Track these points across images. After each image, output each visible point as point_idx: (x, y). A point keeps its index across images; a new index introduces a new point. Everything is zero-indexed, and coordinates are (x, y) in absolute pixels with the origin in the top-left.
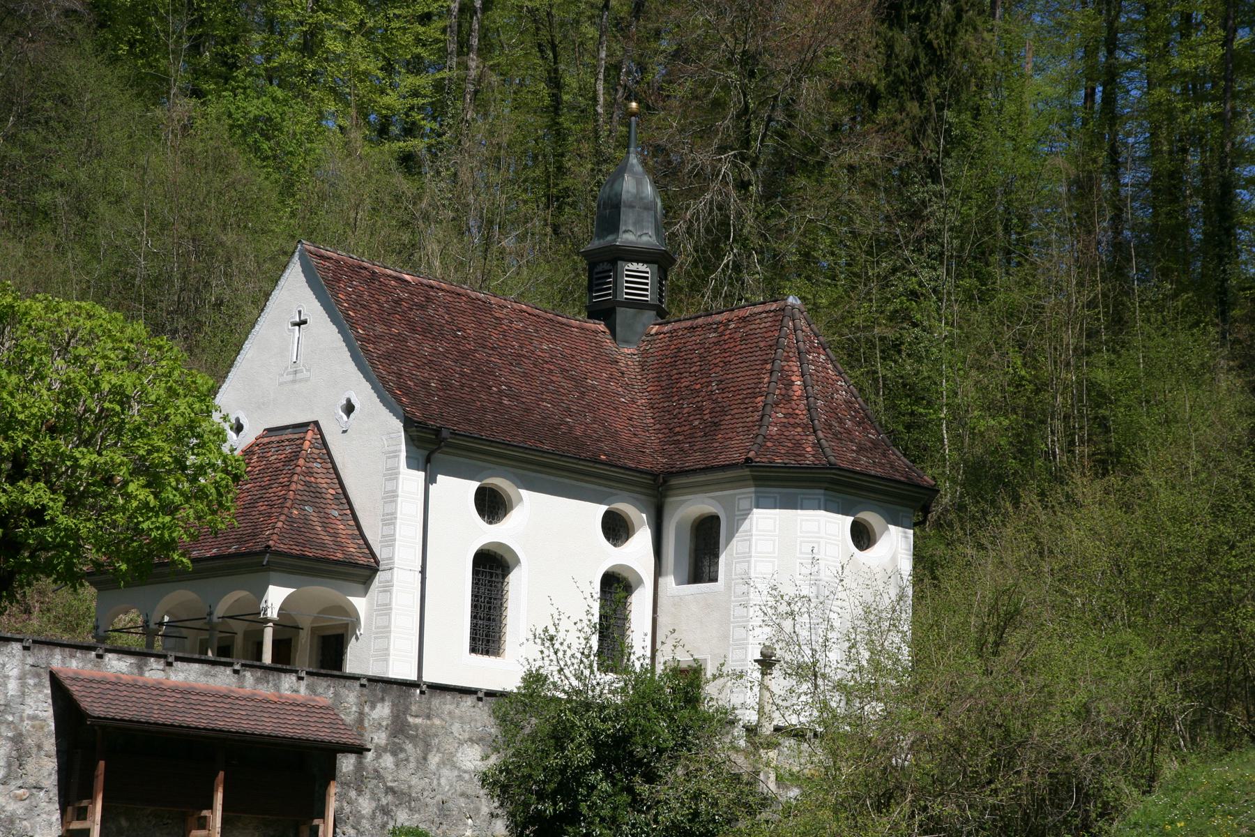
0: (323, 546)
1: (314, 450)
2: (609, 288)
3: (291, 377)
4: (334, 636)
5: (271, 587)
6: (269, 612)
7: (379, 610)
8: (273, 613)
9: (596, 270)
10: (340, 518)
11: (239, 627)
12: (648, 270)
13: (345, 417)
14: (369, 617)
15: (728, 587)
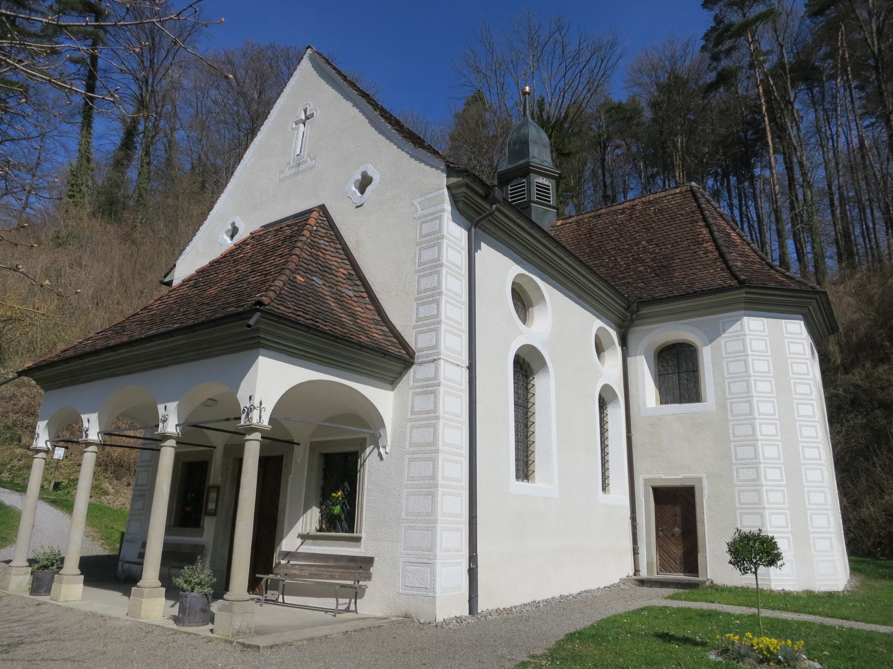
0: (343, 325)
1: (320, 229)
3: (293, 171)
4: (341, 454)
6: (255, 415)
7: (416, 420)
8: (262, 418)
10: (355, 299)
11: (219, 440)
12: (549, 184)
15: (722, 406)
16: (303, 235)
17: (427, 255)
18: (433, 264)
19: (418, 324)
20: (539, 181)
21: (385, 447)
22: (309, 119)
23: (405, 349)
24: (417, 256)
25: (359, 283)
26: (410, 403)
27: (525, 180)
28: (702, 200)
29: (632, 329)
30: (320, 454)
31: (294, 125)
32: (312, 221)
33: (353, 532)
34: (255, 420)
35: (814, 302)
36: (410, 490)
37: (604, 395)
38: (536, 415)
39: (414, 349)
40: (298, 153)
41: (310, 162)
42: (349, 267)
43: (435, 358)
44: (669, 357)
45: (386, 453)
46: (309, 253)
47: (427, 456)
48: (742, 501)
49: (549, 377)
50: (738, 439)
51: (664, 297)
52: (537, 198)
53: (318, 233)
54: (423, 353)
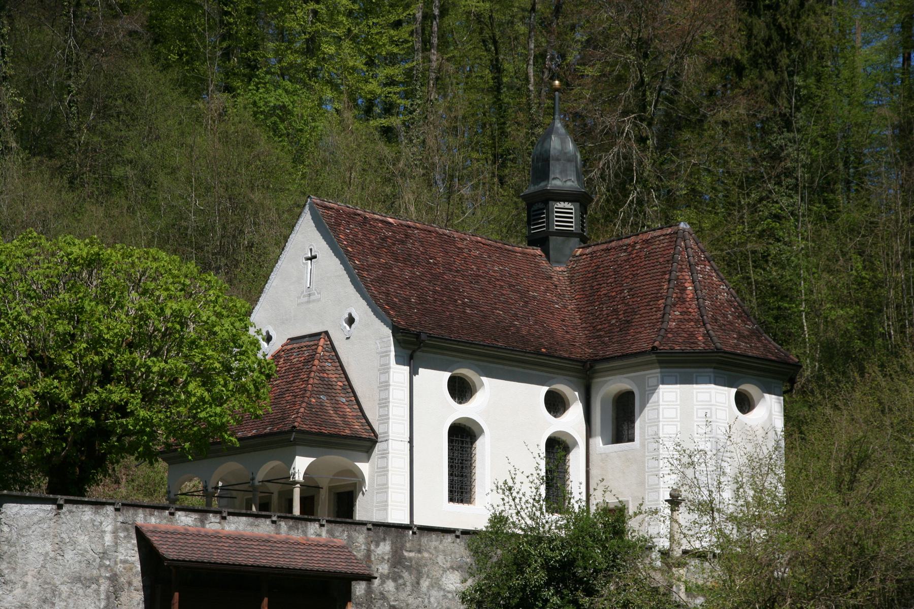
0: (335, 425)
3: (306, 299)
6: (297, 475)
8: (299, 477)
9: (533, 209)
10: (347, 403)
12: (572, 207)
14: (372, 477)
15: (643, 445)
34: (297, 478)
38: (477, 461)
41: (317, 296)
42: (344, 379)
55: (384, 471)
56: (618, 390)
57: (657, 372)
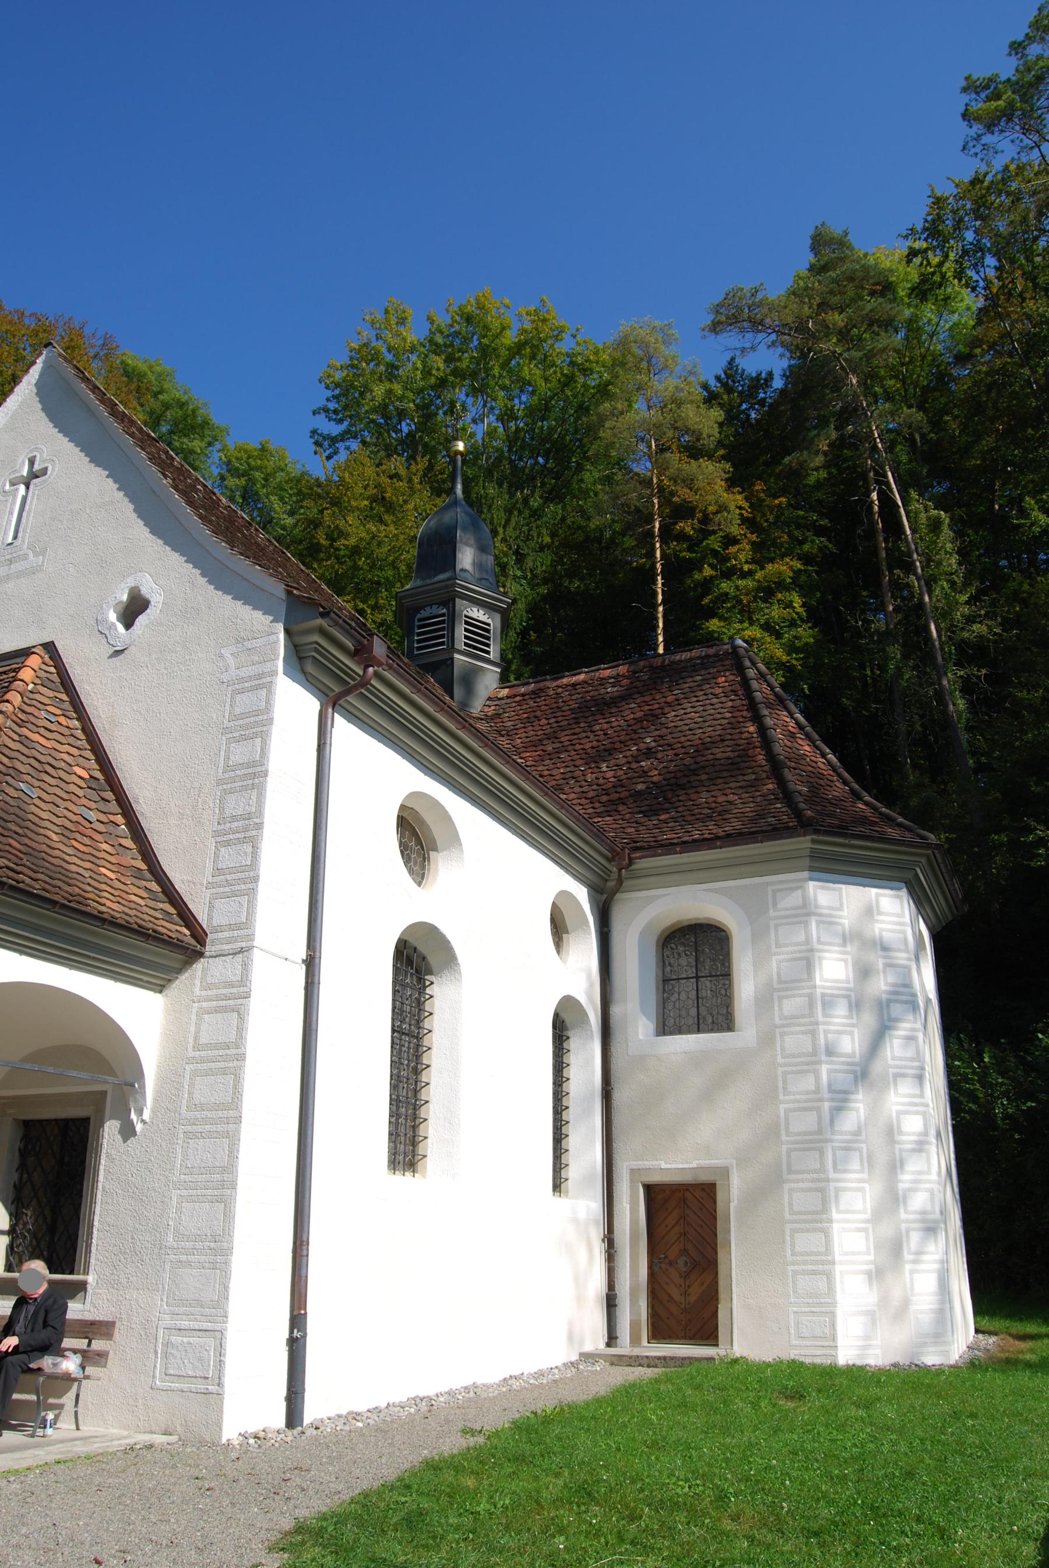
2: (443, 636)
5: (230, 1432)
7: (202, 1060)
9: (419, 616)
10: (101, 828)
12: (489, 621)
13: (120, 628)
14: (170, 1078)
16: (7, 701)
17: (239, 754)
18: (250, 770)
19: (215, 879)
20: (471, 614)
21: (140, 1112)
22: (37, 477)
23: (187, 927)
24: (222, 753)
25: (109, 795)
26: (193, 1029)
27: (444, 611)
28: (751, 673)
29: (618, 896)
30: (14, 1119)
31: (7, 487)
32: (26, 674)
33: (72, 1272)
35: (923, 860)
36: (184, 1193)
37: (563, 1015)
39: (205, 926)
40: (10, 541)
42: (93, 764)
43: (244, 945)
44: (681, 949)
45: (144, 1122)
46: (16, 737)
47: (219, 1128)
48: (795, 1208)
49: (460, 981)
50: (792, 1097)
51: (675, 841)
52: (466, 644)
53: (37, 697)
54: (220, 935)
55: (225, 1058)
56: (674, 920)
57: (806, 874)
